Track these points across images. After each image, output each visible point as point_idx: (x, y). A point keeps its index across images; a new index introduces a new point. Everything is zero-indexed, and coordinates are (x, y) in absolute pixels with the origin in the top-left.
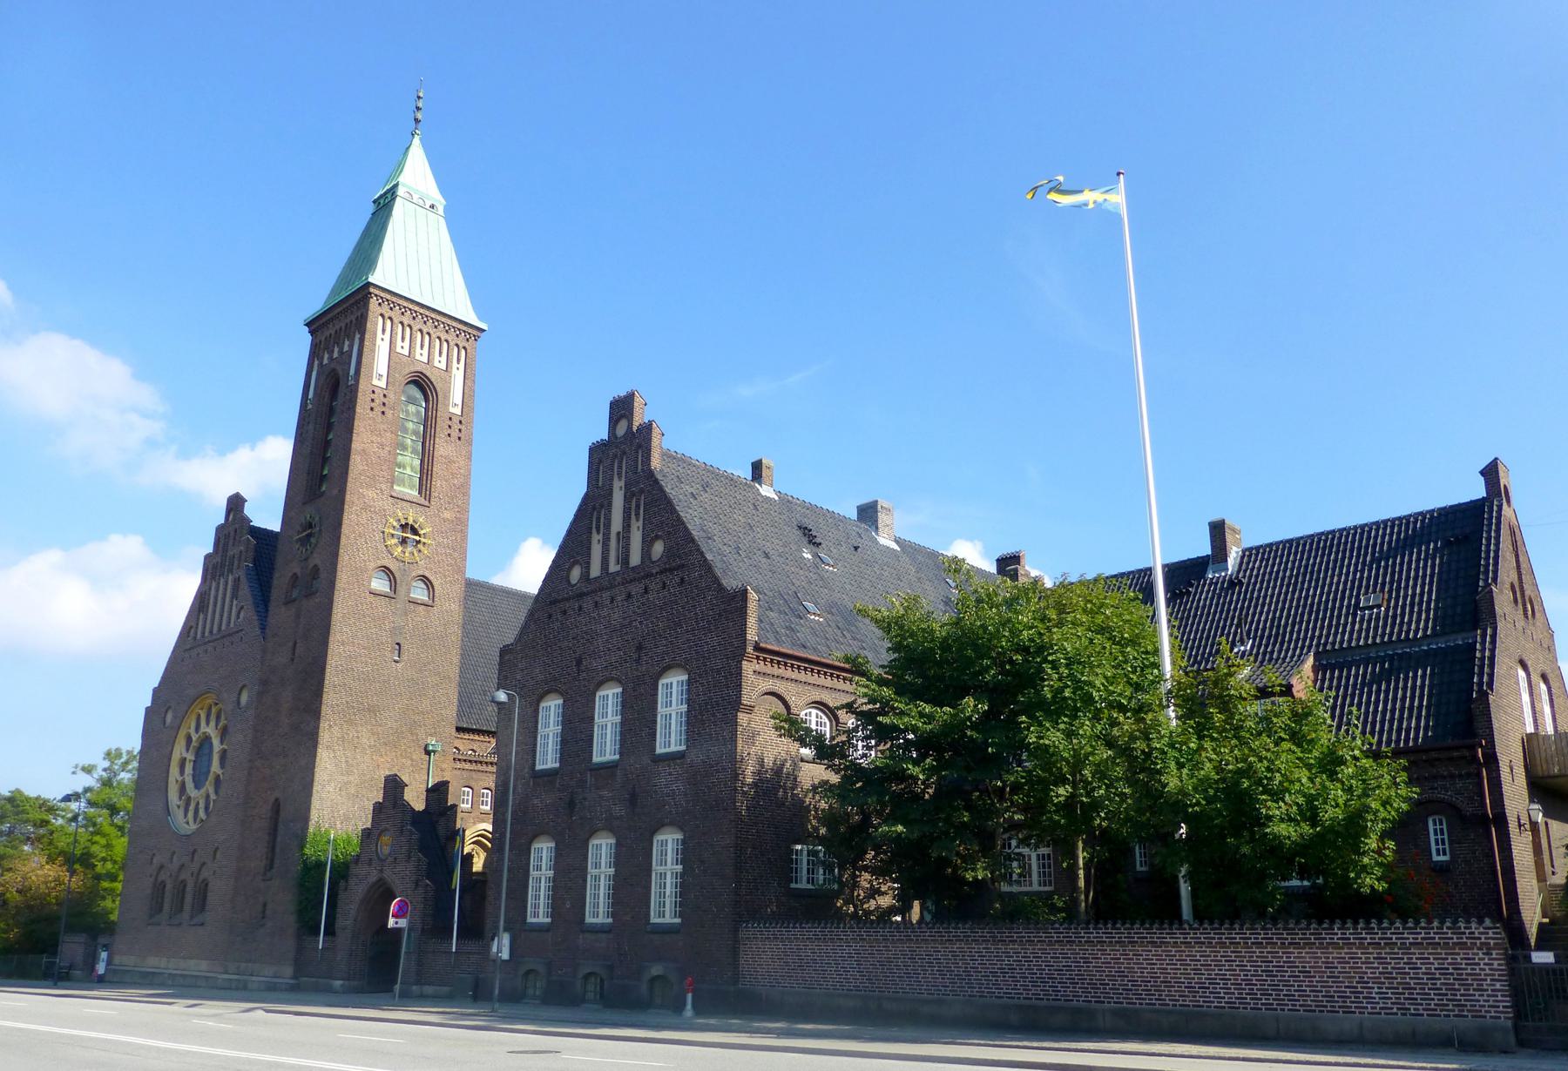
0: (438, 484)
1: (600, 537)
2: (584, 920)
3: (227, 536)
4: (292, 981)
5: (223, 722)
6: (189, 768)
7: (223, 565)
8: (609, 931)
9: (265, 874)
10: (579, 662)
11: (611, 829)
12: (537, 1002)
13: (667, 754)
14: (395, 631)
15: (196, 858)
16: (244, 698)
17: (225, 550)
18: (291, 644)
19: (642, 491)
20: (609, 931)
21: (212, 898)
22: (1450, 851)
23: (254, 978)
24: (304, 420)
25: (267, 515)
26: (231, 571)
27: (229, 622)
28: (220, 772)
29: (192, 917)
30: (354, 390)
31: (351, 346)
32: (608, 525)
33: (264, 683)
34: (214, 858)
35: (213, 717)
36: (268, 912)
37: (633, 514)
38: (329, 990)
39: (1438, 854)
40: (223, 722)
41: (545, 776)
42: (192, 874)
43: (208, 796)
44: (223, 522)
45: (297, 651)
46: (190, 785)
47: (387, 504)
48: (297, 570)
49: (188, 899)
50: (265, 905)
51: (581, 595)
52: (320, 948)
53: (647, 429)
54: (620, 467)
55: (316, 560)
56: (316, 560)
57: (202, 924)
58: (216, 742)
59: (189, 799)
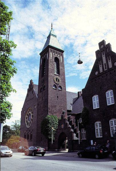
0: (60, 72)
1: (101, 65)
3: (30, 86)
5: (32, 111)
6: (28, 119)
10: (101, 88)
12: (15, 148)
13: (110, 105)
14: (57, 94)
16: (35, 107)
18: (42, 98)
19: (109, 55)
24: (65, 38)
25: (36, 82)
26: (31, 90)
30: (48, 60)
31: (47, 55)
32: (102, 62)
33: (38, 104)
37: (108, 59)
38: (55, 151)
40: (32, 111)
46: (28, 121)
47: (54, 75)
48: (42, 87)
49: (29, 137)
50: (42, 138)
51: (99, 76)
53: (109, 44)
54: (103, 53)
55: (45, 85)
56: (45, 85)
58: (31, 114)
59: (28, 123)
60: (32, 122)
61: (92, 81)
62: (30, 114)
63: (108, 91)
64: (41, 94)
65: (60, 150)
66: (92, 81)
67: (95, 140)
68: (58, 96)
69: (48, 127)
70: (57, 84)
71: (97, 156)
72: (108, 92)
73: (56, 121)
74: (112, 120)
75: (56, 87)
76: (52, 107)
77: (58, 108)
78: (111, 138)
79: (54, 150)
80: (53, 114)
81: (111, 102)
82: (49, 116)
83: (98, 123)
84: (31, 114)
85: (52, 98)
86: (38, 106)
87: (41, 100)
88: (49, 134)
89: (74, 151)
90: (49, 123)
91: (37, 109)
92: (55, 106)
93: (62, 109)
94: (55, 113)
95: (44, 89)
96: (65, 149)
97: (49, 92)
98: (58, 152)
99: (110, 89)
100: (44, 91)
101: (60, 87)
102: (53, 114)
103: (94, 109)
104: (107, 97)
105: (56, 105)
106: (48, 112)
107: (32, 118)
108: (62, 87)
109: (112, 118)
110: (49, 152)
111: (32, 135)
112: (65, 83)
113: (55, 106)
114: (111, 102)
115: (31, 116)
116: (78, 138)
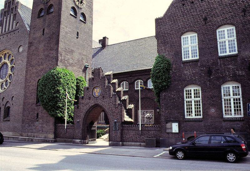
2: (185, 117)
4: (54, 140)
7: (8, 11)
8: (243, 120)
9: (36, 104)
11: (235, 79)
14: (77, 28)
15: (4, 100)
17: (9, 7)
18: (42, 30)
20: (243, 120)
21: (11, 112)
22: (203, 115)
23: (35, 138)
27: (12, 27)
28: (11, 73)
29: (4, 118)
33: (31, 44)
34: (12, 100)
35: (7, 57)
36: (39, 116)
38: (74, 142)
39: (187, 116)
41: (191, 62)
42: (3, 105)
43: (7, 81)
44: (3, 8)
45: (45, 32)
48: (42, 7)
50: (38, 114)
52: (140, 130)
57: (9, 120)
58: (9, 64)
60: (9, 81)
61: (183, 5)
62: (5, 64)
63: (221, 27)
64: (39, 22)
65: (86, 142)
66: (183, 5)
67: (182, 122)
68: (78, 32)
69: (58, 91)
70: (78, 7)
71: (231, 157)
72: (186, 36)
73: (73, 83)
74: (189, 89)
75: (75, 13)
76: (66, 51)
77: (76, 56)
78: (224, 121)
79: (71, 142)
80: (66, 67)
81: (228, 50)
82: (60, 68)
83: (231, 86)
84: (9, 64)
85: (66, 33)
86: (29, 47)
87: (39, 34)
88: (60, 107)
89: (125, 143)
90: (60, 83)
91: (26, 54)
92: (72, 52)
93: (84, 61)
94: (71, 65)
95: (48, 13)
96: (95, 140)
97: (62, 19)
98: (83, 143)
99: (228, 24)
100: (48, 17)
101: (83, 15)
102: (66, 67)
103: (183, 60)
104: (218, 40)
105: (75, 49)
106: (57, 60)
107: (10, 72)
108: (87, 16)
109: (229, 81)
110: (60, 146)
111: (9, 108)
112: (92, 10)
113: (72, 52)
114: (228, 50)
115: (9, 69)
116: (132, 119)
